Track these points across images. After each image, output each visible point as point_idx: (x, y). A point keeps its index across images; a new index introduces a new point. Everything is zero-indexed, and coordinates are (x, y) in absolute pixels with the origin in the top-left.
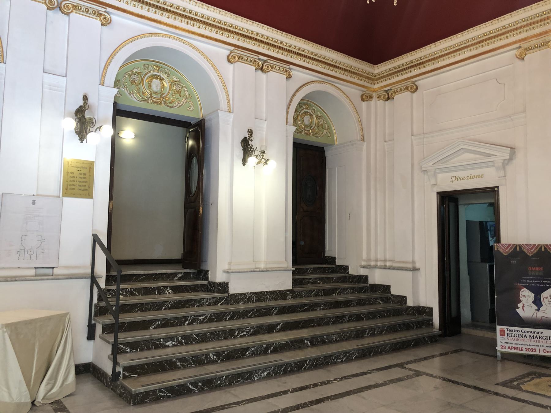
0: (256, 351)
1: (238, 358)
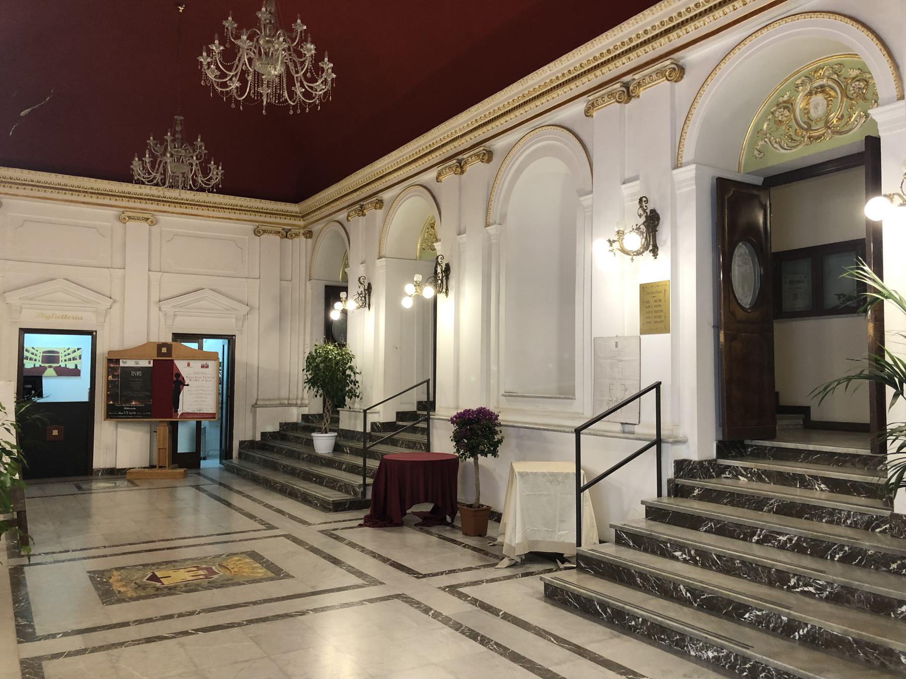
0: (767, 619)
1: (729, 616)
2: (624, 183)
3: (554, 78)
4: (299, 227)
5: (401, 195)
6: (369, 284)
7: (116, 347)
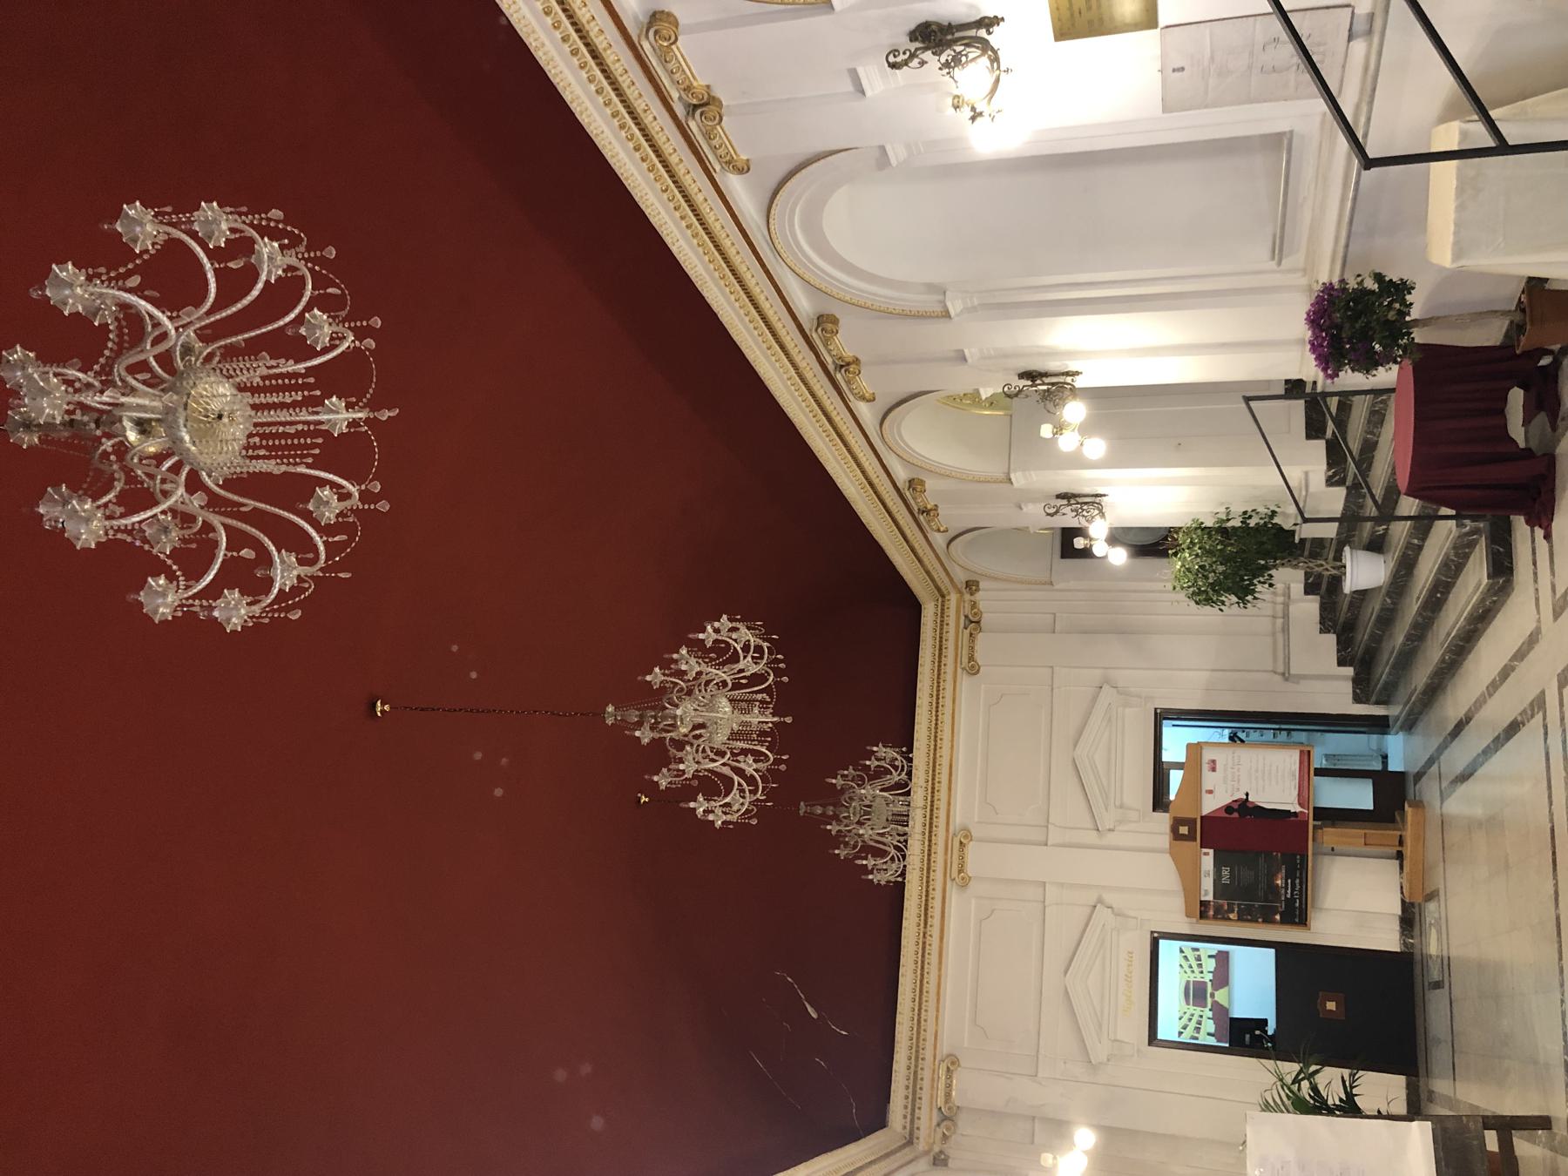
2: (863, 92)
3: (689, 232)
4: (960, 601)
5: (896, 455)
6: (1059, 496)
7: (1178, 903)
